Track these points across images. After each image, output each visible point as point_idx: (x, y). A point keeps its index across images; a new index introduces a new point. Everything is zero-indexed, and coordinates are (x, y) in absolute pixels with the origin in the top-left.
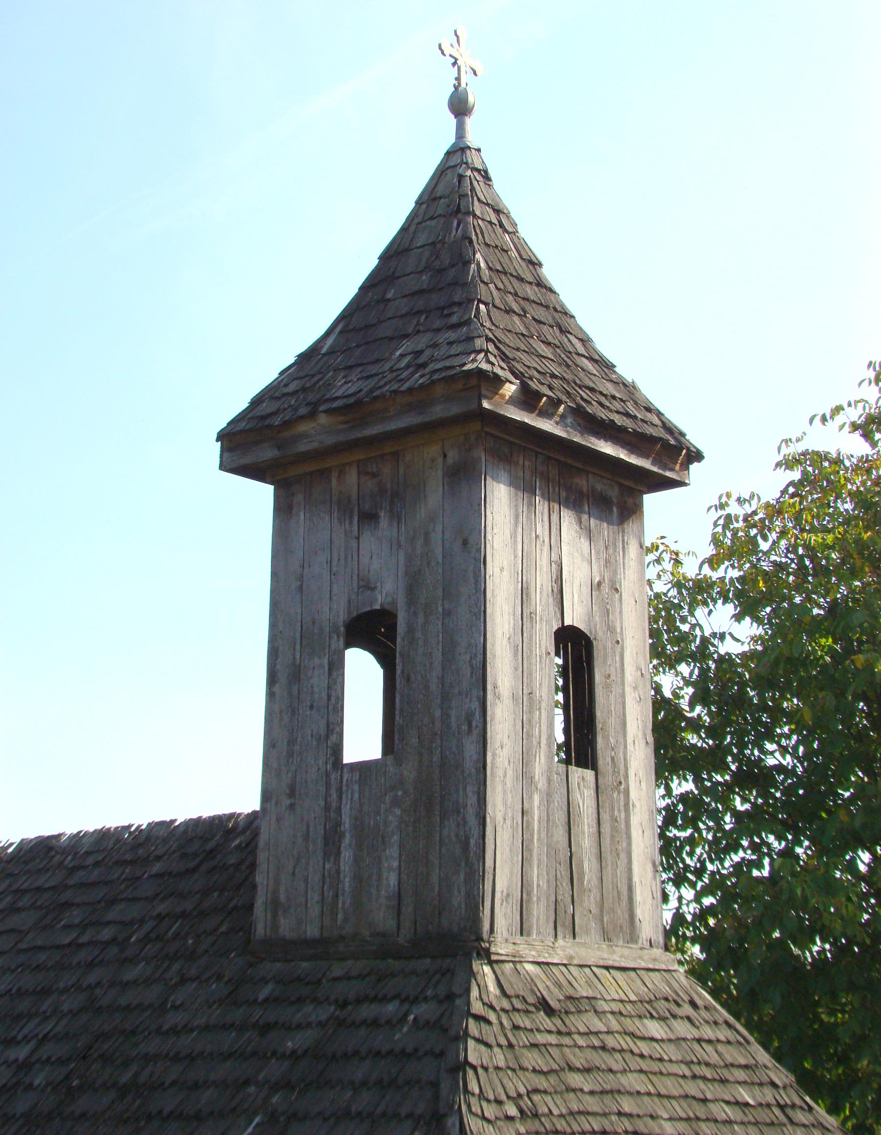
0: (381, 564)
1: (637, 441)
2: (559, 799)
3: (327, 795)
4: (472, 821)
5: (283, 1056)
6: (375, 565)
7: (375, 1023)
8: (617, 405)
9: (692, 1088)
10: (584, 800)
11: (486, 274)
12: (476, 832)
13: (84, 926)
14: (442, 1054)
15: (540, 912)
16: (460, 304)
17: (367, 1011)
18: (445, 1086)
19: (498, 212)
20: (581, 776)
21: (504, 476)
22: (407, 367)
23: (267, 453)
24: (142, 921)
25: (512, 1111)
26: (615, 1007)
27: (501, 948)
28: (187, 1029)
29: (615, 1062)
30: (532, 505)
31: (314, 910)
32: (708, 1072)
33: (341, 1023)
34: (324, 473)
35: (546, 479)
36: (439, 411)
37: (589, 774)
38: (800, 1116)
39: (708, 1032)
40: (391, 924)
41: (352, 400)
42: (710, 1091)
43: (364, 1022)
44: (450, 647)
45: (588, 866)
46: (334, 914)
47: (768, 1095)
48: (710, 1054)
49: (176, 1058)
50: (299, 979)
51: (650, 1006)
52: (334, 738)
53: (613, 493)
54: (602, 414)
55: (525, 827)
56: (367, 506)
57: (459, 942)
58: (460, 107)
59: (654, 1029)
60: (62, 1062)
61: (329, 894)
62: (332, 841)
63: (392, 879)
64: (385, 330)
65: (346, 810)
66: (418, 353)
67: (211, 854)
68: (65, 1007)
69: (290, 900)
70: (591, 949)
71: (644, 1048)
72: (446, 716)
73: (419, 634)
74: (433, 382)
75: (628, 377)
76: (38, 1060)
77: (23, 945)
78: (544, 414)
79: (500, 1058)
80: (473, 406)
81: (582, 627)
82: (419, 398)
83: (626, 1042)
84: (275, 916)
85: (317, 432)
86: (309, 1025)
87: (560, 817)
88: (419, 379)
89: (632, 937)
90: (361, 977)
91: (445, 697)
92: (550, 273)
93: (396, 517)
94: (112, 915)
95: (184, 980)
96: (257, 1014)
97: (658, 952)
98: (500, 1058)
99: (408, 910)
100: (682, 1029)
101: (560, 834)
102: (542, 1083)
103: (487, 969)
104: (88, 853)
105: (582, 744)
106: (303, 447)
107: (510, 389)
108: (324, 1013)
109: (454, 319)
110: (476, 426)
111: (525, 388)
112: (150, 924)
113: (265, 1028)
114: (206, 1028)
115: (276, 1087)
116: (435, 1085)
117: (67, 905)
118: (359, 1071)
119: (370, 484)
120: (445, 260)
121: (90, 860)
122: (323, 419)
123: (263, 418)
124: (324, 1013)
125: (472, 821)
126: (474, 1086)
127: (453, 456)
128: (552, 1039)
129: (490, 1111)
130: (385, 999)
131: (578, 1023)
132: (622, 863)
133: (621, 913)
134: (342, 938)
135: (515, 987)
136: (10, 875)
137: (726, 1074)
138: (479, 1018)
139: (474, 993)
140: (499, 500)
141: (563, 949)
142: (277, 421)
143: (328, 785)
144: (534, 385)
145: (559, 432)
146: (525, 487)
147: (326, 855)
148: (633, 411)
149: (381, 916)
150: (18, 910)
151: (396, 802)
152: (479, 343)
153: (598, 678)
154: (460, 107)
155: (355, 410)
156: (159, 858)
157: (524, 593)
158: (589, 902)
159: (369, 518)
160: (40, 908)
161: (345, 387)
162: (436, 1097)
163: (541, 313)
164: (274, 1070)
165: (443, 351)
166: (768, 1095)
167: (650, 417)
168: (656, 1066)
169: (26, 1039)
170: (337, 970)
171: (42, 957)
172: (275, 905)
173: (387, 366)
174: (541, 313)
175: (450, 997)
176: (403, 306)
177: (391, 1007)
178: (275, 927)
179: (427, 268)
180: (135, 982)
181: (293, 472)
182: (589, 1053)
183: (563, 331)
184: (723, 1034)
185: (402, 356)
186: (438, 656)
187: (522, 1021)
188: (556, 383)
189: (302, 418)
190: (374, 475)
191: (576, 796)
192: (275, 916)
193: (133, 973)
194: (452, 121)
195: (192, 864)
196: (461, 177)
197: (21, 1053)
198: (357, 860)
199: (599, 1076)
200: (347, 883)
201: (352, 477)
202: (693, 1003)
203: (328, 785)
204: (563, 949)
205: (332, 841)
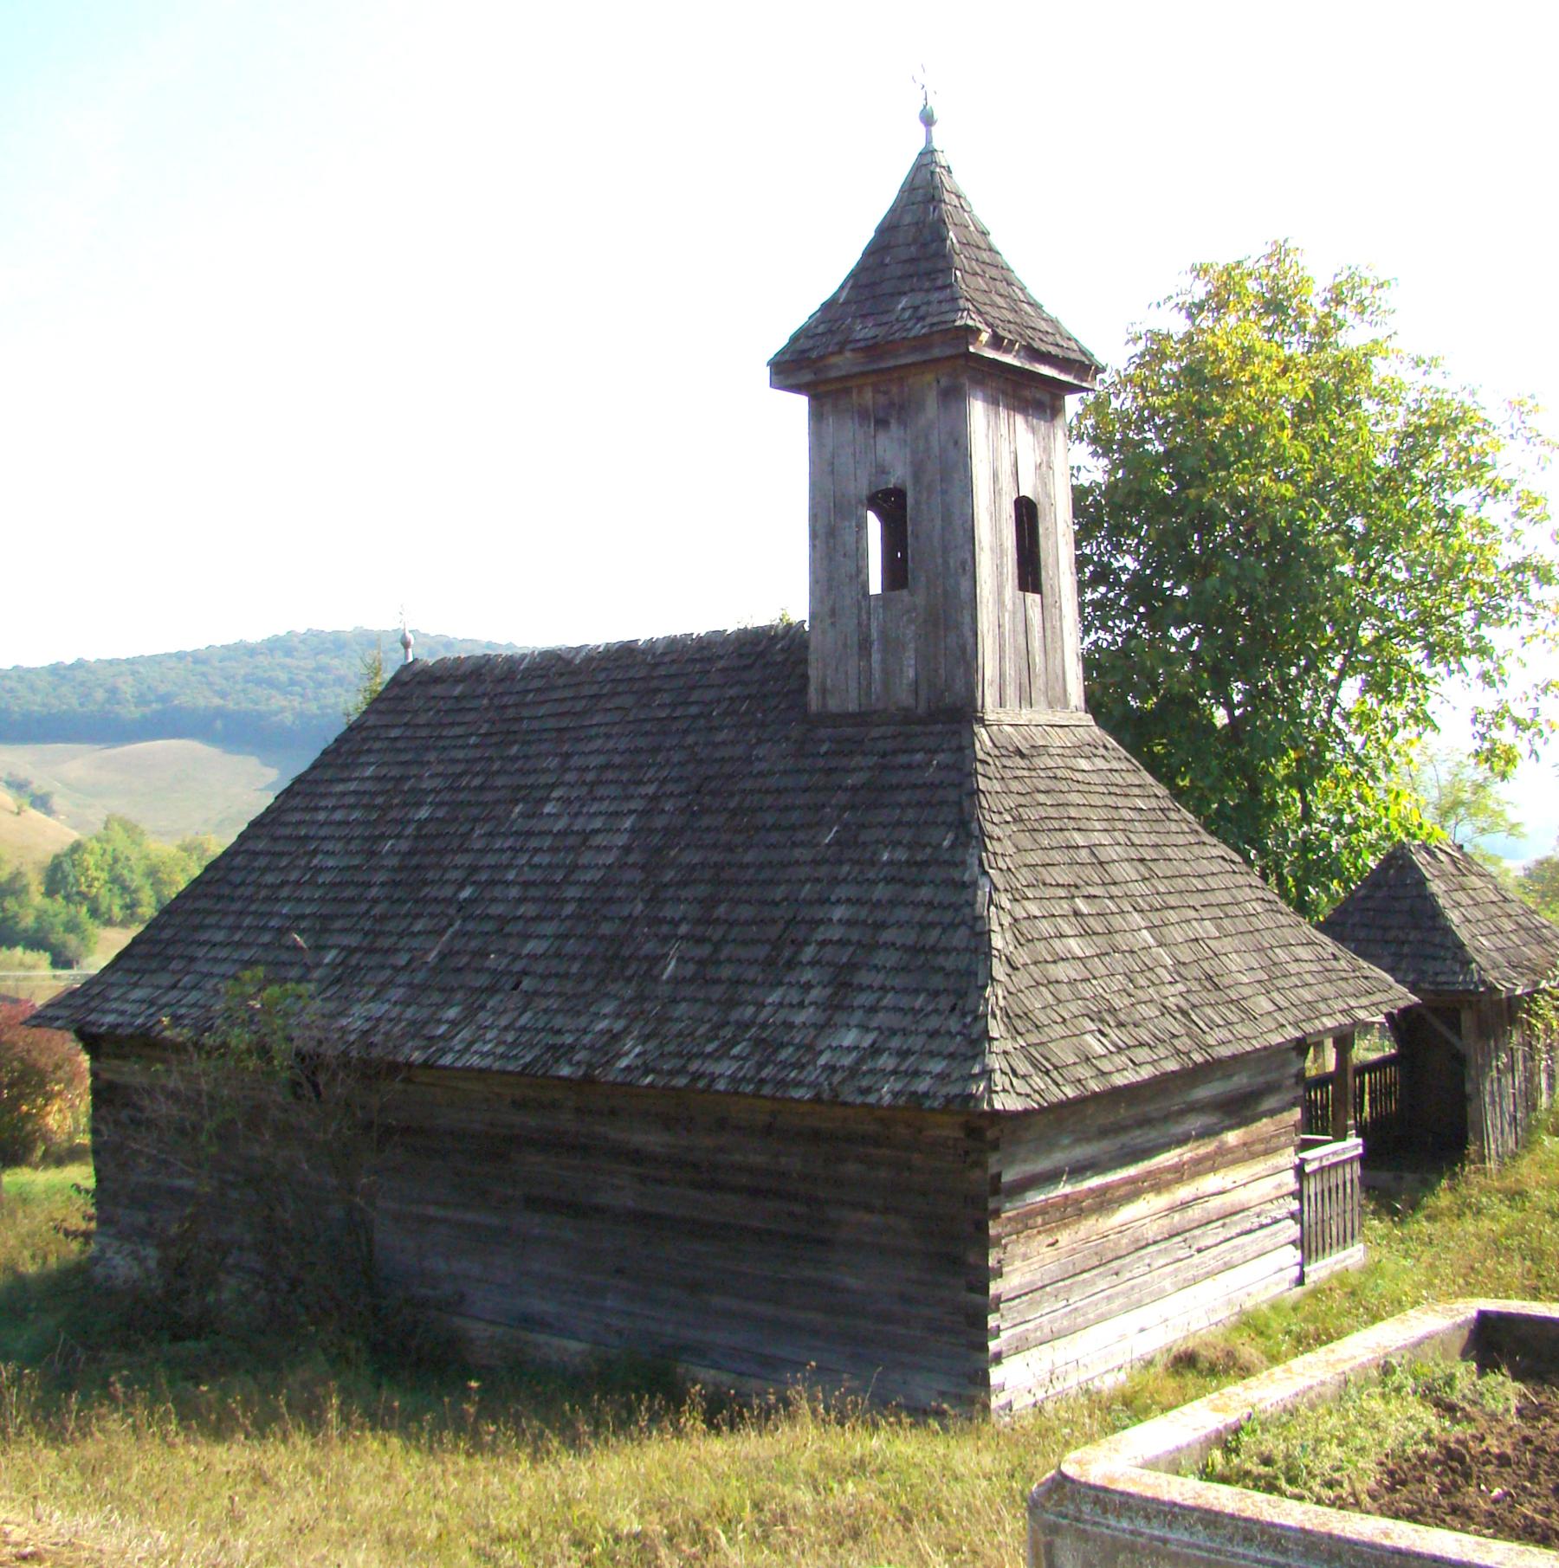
0: (893, 456)
1: (1063, 364)
2: (1020, 616)
3: (859, 616)
4: (969, 634)
5: (846, 789)
6: (888, 456)
7: (909, 767)
8: (1050, 339)
9: (1110, 801)
10: (1035, 615)
11: (957, 246)
12: (971, 640)
13: (674, 706)
14: (960, 785)
15: (1011, 692)
16: (942, 271)
17: (903, 759)
18: (966, 803)
19: (959, 197)
20: (1032, 598)
21: (980, 394)
22: (910, 319)
23: (807, 377)
24: (719, 701)
25: (1009, 818)
26: (1060, 751)
27: (990, 716)
28: (771, 773)
29: (1063, 786)
30: (997, 414)
31: (854, 694)
32: (1118, 791)
33: (883, 768)
34: (847, 391)
35: (1004, 393)
36: (936, 352)
37: (1037, 597)
38: (1173, 815)
39: (1115, 765)
40: (911, 702)
41: (870, 343)
42: (1120, 802)
43: (902, 766)
44: (947, 517)
45: (1038, 659)
46: (868, 694)
47: (1154, 803)
48: (1117, 779)
49: (767, 792)
50: (848, 740)
51: (1079, 750)
52: (862, 577)
53: (1046, 398)
54: (1044, 348)
55: (1001, 636)
56: (881, 415)
57: (962, 713)
58: (928, 120)
59: (1083, 764)
60: (681, 795)
61: (864, 683)
62: (864, 646)
63: (911, 673)
64: (887, 287)
65: (874, 625)
66: (916, 308)
67: (761, 654)
68: (675, 760)
69: (835, 685)
70: (1040, 714)
71: (1079, 776)
72: (946, 563)
73: (923, 507)
74: (932, 334)
75: (1054, 315)
76: (664, 794)
77: (631, 718)
78: (1007, 351)
79: (997, 786)
80: (962, 350)
81: (1030, 496)
82: (922, 343)
83: (1068, 774)
84: (824, 698)
85: (845, 363)
86: (862, 769)
87: (1021, 628)
88: (919, 329)
89: (1066, 706)
90: (894, 737)
91: (945, 549)
92: (995, 240)
93: (903, 423)
94: (695, 696)
95: (760, 742)
96: (821, 763)
97: (1081, 714)
98: (997, 786)
99: (923, 693)
100: (1100, 763)
101: (1021, 639)
102: (1022, 800)
103: (983, 730)
104: (664, 654)
105: (1030, 574)
106: (833, 374)
107: (985, 337)
108: (872, 760)
109: (939, 283)
110: (962, 362)
111: (995, 335)
112: (725, 705)
113: (830, 771)
114: (785, 772)
115: (844, 809)
116: (959, 804)
117: (658, 690)
118: (903, 798)
119: (882, 399)
120: (918, 244)
121: (667, 659)
122: (848, 354)
123: (804, 351)
124: (872, 760)
125: (969, 634)
126: (984, 804)
127: (944, 382)
128: (1026, 773)
129: (996, 818)
130: (914, 751)
131: (1040, 762)
133: (1059, 690)
134: (875, 712)
135: (1001, 741)
136: (605, 669)
137: (1127, 790)
138: (983, 762)
139: (978, 746)
140: (978, 410)
141: (1026, 715)
142: (814, 355)
143: (860, 609)
144: (1001, 332)
145: (1016, 363)
146: (993, 402)
147: (860, 658)
148: (1061, 342)
149: (904, 697)
150: (619, 694)
151: (911, 621)
152: (962, 303)
153: (1041, 531)
154: (928, 120)
155: (872, 349)
156: (721, 657)
157: (995, 476)
158: (1039, 683)
159: (882, 423)
160: (635, 693)
161: (864, 331)
162: (961, 810)
163: (994, 272)
164: (842, 798)
165: (933, 308)
166: (1154, 803)
167: (1073, 345)
168: (1086, 788)
169: (651, 781)
170: (876, 732)
171: (648, 727)
172: (824, 691)
173: (894, 317)
174: (994, 272)
175: (960, 749)
176: (898, 271)
177: (919, 757)
178: (824, 705)
179: (915, 241)
180: (724, 743)
181: (822, 389)
182: (1048, 781)
183: (1009, 284)
184: (1124, 765)
185: (904, 309)
186: (938, 523)
187: (1008, 763)
188: (1012, 327)
189: (832, 354)
190: (886, 393)
191: (1030, 612)
192: (824, 698)
193: (721, 737)
194: (922, 128)
195: (749, 661)
196: (933, 173)
197: (650, 789)
198: (883, 661)
199: (1056, 796)
200: (877, 675)
201: (868, 395)
202: (1105, 747)
203: (860, 609)
204: (1026, 715)
205: (864, 646)
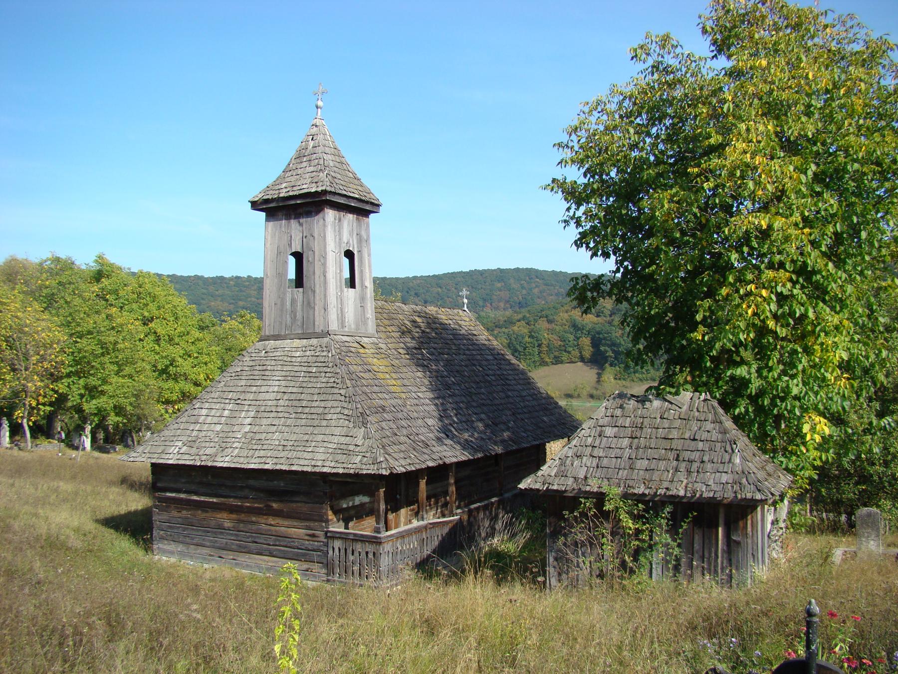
132: (311, 312)
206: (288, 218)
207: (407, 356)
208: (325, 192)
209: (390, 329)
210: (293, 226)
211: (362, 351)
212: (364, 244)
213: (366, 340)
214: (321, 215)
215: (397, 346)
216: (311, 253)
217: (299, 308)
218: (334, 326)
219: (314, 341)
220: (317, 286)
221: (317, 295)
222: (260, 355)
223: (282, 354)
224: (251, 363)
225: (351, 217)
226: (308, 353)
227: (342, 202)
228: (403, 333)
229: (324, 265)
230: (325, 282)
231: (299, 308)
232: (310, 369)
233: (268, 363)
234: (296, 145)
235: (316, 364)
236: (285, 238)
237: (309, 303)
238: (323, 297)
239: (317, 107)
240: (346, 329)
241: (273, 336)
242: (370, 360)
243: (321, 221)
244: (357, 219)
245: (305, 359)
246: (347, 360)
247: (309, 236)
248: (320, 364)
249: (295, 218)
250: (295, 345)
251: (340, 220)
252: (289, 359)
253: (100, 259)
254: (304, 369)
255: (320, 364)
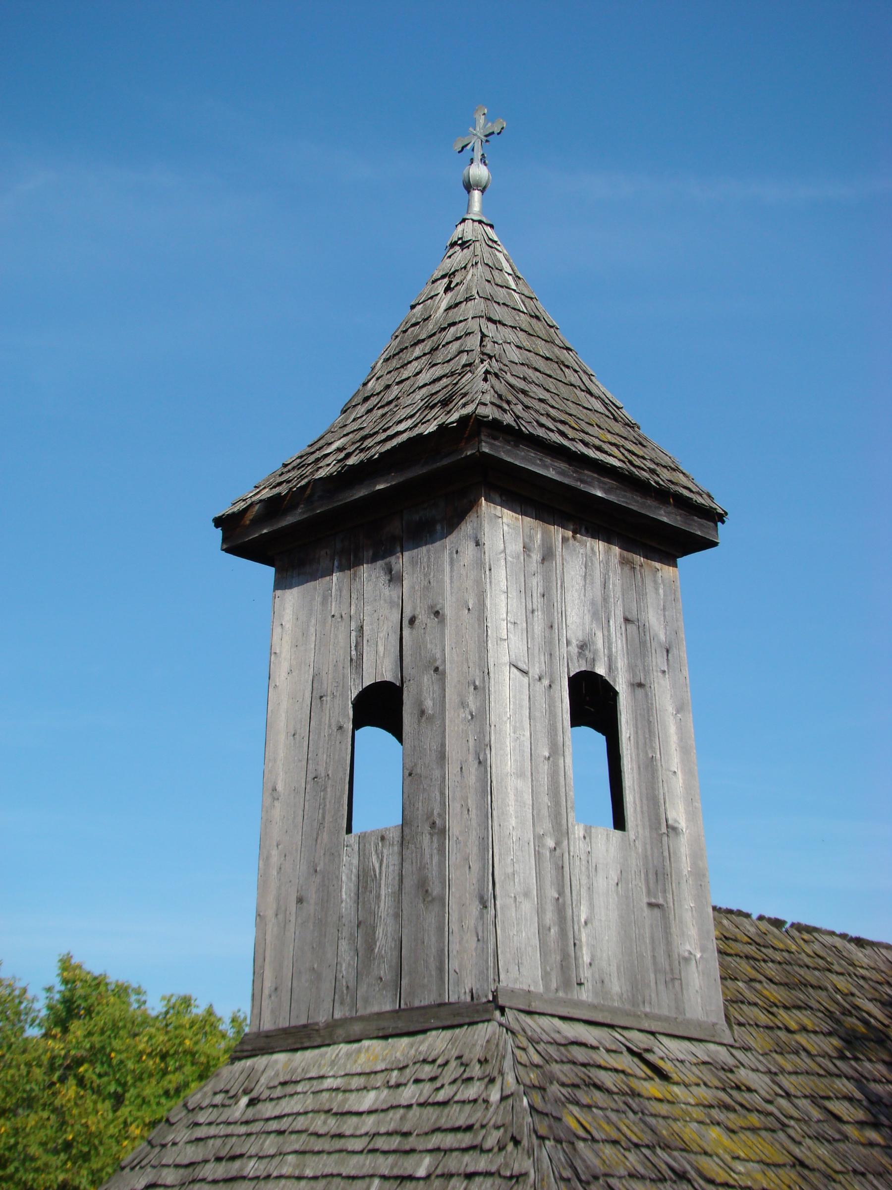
132: (430, 919)
206: (350, 560)
207: (873, 1135)
208: (473, 426)
209: (790, 1019)
210: (368, 588)
211: (653, 1088)
212: (658, 661)
213: (676, 1048)
214: (467, 527)
215: (821, 1086)
216: (427, 679)
217: (385, 906)
218: (524, 970)
219: (437, 1042)
220: (454, 808)
221: (451, 845)
222: (226, 1114)
223: (310, 1102)
224: (191, 1153)
225: (600, 552)
226: (409, 1094)
227: (551, 474)
228: (851, 1040)
229: (480, 718)
230: (486, 789)
231: (385, 906)
232: (407, 1165)
233: (251, 1147)
234: (401, 315)
235: (435, 1141)
236: (341, 640)
237: (423, 887)
238: (473, 850)
239: (469, 187)
240: (585, 995)
241: (286, 1032)
242: (690, 1131)
243: (468, 551)
244: (624, 562)
245: (391, 1121)
246: (572, 1118)
247: (423, 618)
248: (449, 1140)
249: (373, 560)
250: (362, 1063)
251: (547, 556)
252: (332, 1124)
253: (139, 987)
254: (385, 1165)
255: (449, 1140)
